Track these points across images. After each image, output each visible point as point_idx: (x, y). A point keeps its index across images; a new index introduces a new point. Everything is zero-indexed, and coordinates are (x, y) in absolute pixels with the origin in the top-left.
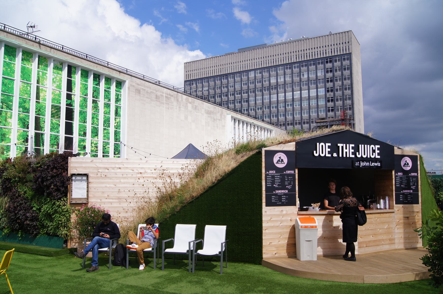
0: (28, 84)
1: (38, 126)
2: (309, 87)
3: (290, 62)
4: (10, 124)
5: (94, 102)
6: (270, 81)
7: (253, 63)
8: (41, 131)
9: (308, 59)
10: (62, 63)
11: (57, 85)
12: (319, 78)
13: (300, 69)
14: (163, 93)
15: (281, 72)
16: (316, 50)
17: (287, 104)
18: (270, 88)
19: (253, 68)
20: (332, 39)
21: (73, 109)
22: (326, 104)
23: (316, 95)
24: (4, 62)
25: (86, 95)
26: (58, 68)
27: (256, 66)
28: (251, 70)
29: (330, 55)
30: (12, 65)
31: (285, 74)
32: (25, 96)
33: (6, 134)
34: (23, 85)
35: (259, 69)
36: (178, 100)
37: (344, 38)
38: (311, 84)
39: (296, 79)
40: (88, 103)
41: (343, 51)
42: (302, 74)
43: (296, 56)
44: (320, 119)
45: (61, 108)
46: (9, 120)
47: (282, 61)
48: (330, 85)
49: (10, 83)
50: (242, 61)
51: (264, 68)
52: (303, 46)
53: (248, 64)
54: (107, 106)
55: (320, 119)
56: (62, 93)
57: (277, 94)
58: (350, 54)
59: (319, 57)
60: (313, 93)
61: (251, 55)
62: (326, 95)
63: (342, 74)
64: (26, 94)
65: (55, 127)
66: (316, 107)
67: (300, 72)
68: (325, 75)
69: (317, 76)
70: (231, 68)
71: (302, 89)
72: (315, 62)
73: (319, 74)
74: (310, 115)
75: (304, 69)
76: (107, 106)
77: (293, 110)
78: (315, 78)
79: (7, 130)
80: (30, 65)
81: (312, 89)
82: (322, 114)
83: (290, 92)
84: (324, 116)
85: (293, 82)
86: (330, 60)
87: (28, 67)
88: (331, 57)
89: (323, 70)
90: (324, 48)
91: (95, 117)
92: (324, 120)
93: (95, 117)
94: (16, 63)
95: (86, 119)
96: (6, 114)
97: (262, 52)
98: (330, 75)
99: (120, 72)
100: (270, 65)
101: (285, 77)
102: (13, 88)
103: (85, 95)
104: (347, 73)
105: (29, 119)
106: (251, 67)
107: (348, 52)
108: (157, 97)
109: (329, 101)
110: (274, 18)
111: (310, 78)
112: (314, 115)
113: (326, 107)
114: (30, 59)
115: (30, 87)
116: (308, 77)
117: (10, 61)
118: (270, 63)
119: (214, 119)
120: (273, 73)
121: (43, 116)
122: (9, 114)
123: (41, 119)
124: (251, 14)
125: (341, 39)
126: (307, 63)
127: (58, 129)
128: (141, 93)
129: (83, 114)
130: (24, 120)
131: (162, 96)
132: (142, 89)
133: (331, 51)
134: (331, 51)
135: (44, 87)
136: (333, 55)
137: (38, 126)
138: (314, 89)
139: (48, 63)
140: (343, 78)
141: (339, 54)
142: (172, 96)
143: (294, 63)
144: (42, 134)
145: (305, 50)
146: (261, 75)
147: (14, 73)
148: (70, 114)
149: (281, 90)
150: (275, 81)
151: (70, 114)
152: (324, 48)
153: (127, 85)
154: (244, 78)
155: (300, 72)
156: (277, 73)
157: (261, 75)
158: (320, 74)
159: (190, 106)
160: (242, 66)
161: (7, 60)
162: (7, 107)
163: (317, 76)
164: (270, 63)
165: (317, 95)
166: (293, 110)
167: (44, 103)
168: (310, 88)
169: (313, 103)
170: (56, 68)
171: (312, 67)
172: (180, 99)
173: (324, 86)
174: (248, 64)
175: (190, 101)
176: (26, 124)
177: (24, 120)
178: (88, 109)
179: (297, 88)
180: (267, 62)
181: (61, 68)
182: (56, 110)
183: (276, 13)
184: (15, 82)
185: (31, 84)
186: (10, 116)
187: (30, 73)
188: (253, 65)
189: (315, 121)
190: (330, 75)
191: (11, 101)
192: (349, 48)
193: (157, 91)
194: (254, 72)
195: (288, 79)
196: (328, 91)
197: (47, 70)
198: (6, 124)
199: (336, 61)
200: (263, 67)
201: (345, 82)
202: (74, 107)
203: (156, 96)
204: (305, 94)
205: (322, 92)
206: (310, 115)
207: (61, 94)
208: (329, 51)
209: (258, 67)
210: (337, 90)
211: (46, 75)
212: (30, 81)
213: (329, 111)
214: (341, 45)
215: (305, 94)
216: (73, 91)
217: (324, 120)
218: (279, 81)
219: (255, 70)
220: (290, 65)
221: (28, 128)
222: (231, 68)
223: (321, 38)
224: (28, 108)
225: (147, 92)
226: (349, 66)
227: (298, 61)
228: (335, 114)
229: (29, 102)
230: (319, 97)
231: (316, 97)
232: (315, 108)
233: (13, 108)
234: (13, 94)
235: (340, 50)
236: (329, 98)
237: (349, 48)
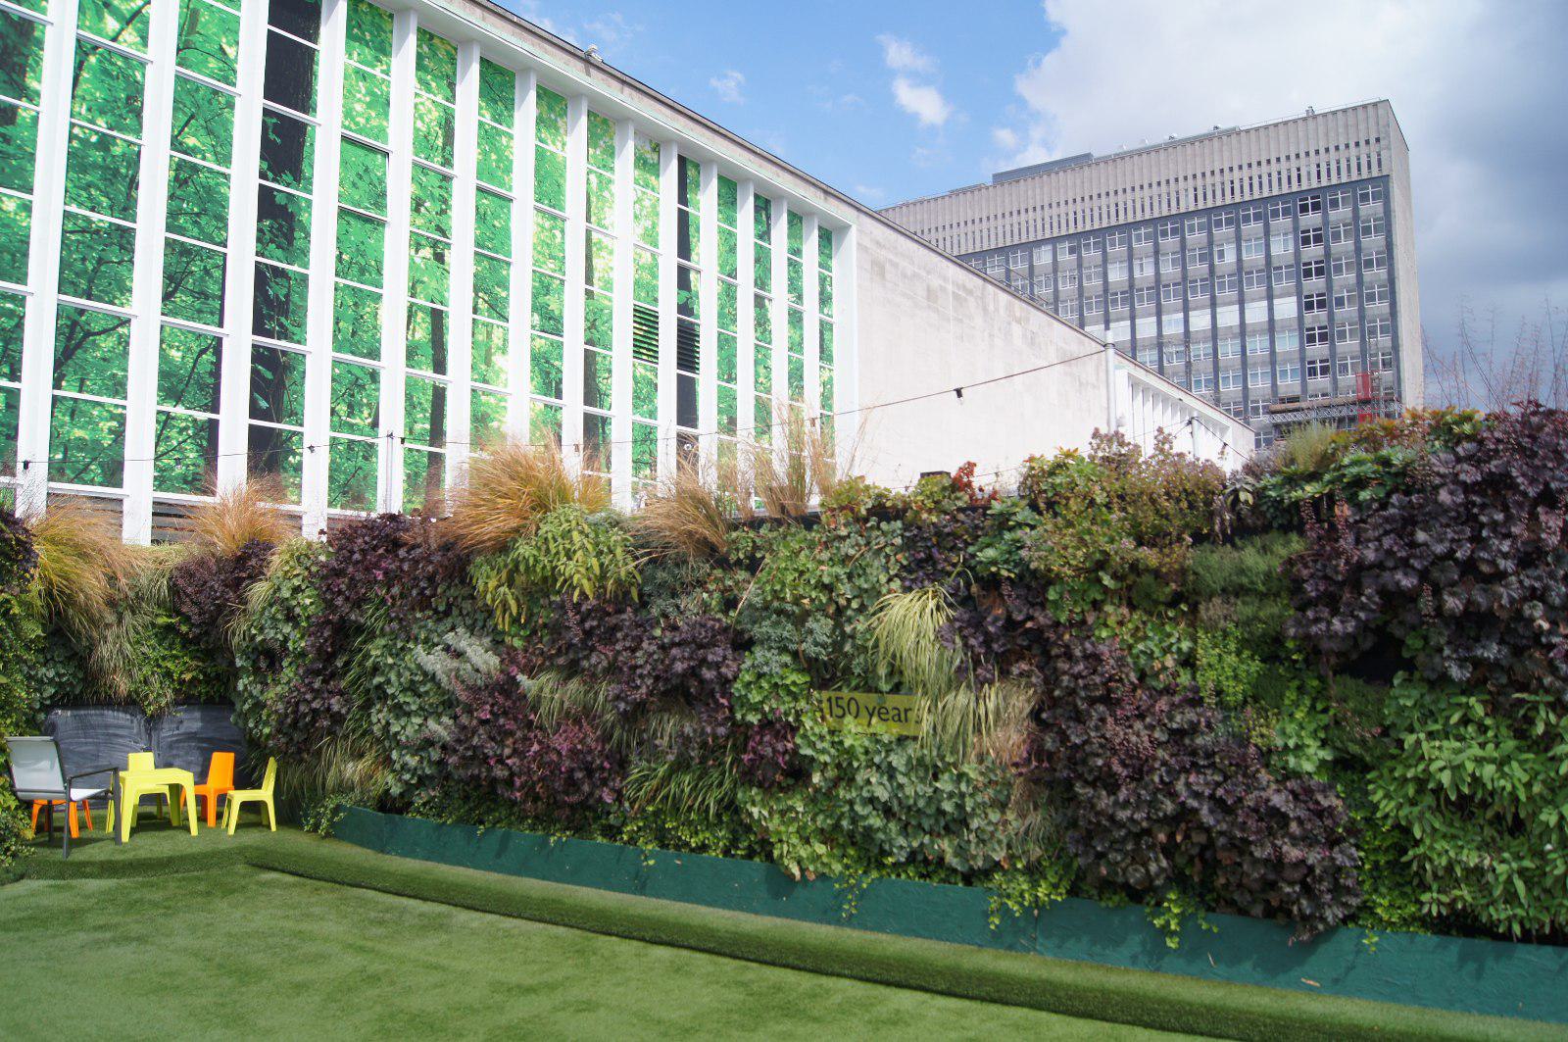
0: (554, 217)
1: (593, 393)
2: (1241, 293)
3: (1174, 212)
4: (503, 376)
5: (759, 302)
6: (1105, 275)
7: (1047, 219)
8: (601, 407)
9: (1238, 199)
10: (658, 145)
11: (646, 229)
12: (1275, 264)
13: (1210, 234)
14: (945, 279)
15: (1143, 246)
16: (1264, 168)
19: (1047, 236)
20: (1321, 130)
21: (692, 323)
22: (1302, 350)
23: (1265, 318)
24: (481, 124)
25: (733, 274)
26: (645, 162)
27: (1001, 239)
28: (1039, 243)
29: (1315, 184)
30: (504, 140)
31: (1157, 252)
32: (548, 268)
33: (488, 415)
34: (540, 221)
35: (1069, 237)
36: (985, 310)
37: (1362, 127)
40: (739, 304)
41: (1359, 169)
42: (1216, 249)
44: (1282, 401)
45: (660, 320)
46: (497, 359)
47: (1071, 223)
48: (1314, 284)
49: (498, 210)
50: (1007, 214)
51: (1086, 234)
52: (1216, 157)
53: (1031, 222)
54: (796, 318)
55: (1282, 401)
56: (660, 260)
57: (1133, 319)
58: (1385, 179)
59: (1275, 192)
60: (1256, 313)
61: (1038, 191)
62: (1300, 318)
63: (1358, 249)
64: (552, 257)
65: (644, 394)
66: (1268, 359)
67: (1211, 243)
68: (1297, 253)
69: (1268, 256)
70: (970, 235)
72: (1264, 209)
73: (1277, 249)
74: (1274, 385)
75: (1224, 232)
76: (796, 318)
79: (491, 399)
80: (559, 145)
81: (1253, 300)
82: (1289, 385)
83: (1177, 311)
84: (1297, 391)
85: (1184, 277)
86: (1315, 200)
87: (552, 153)
88: (1316, 193)
89: (1291, 236)
90: (1294, 163)
91: (762, 360)
92: (1296, 405)
93: (762, 360)
94: (515, 131)
95: (735, 366)
96: (489, 335)
97: (1078, 182)
98: (1313, 252)
99: (826, 192)
100: (1105, 225)
101: (1157, 264)
102: (506, 230)
103: (729, 275)
104: (1373, 243)
105: (560, 357)
106: (1016, 237)
107: (1375, 173)
108: (930, 294)
109: (1311, 339)
110: (1021, 102)
111: (1245, 265)
112: (1259, 385)
113: (1302, 359)
114: (560, 123)
115: (562, 231)
116: (1239, 260)
117: (496, 121)
118: (1105, 216)
119: (1081, 384)
120: (1117, 250)
121: (605, 347)
122: (497, 334)
123: (599, 359)
124: (948, 94)
125: (1352, 130)
126: (1235, 213)
127: (651, 401)
128: (888, 276)
129: (726, 344)
130: (547, 362)
131: (943, 289)
132: (891, 261)
133: (1319, 172)
134: (1319, 172)
135: (606, 235)
136: (1324, 183)
137: (593, 393)
138: (1261, 299)
139: (616, 143)
140: (1361, 263)
141: (1344, 180)
142: (970, 292)
143: (1189, 214)
144: (604, 421)
145: (1226, 171)
146: (1074, 257)
147: (508, 171)
148: (687, 339)
149: (1145, 306)
150: (1125, 277)
151: (687, 339)
152: (1294, 163)
153: (853, 236)
154: (1019, 266)
155: (1211, 243)
156: (1130, 249)
157: (1074, 257)
158: (1282, 248)
159: (1016, 329)
160: (1008, 228)
161: (487, 119)
162: (491, 306)
163: (1268, 256)
164: (1105, 216)
165: (1187, 331)
167: (606, 297)
168: (1138, 313)
169: (1258, 346)
170: (641, 163)
171: (1254, 228)
172: (991, 308)
173: (1293, 290)
174: (1031, 222)
175: (1018, 314)
176: (552, 376)
177: (547, 362)
178: (738, 329)
181: (653, 165)
182: (646, 321)
183: (1024, 87)
184: (514, 206)
185: (564, 220)
186: (500, 343)
187: (561, 176)
188: (1047, 226)
189: (1264, 407)
190: (1313, 252)
191: (504, 284)
192: (1379, 161)
193: (928, 273)
194: (1050, 247)
195: (1169, 271)
196: (1309, 306)
197: (612, 169)
198: (490, 375)
199: (1334, 204)
200: (1080, 230)
201: (1368, 275)
202: (698, 318)
203: (929, 290)
204: (1228, 317)
205: (1287, 308)
206: (1245, 388)
207: (657, 265)
209: (1063, 233)
210: (1340, 302)
211: (612, 187)
212: (562, 209)
213: (1312, 372)
214: (1353, 150)
215: (1228, 317)
216: (694, 256)
217: (1296, 405)
218: (1137, 274)
219: (1053, 241)
220: (1178, 221)
221: (559, 395)
222: (970, 235)
223: (1262, 132)
224: (557, 313)
225: (904, 276)
226: (1380, 219)
227: (1201, 206)
228: (1335, 381)
229: (561, 293)
230: (1278, 327)
231: (1266, 326)
232: (1263, 364)
233: (512, 311)
234: (508, 254)
235: (1349, 166)
237: (1379, 161)
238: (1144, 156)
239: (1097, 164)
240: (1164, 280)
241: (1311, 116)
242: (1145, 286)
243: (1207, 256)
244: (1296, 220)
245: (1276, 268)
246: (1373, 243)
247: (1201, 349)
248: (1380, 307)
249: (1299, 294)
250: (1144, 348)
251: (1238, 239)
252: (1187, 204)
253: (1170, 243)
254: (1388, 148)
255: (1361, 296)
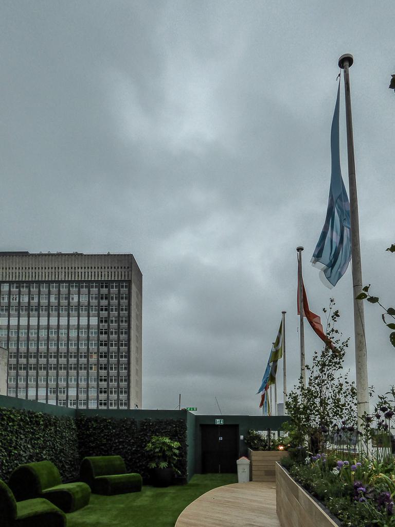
17: (91, 332)
18: (29, 308)
27: (120, 277)
38: (82, 311)
39: (64, 302)
43: (65, 273)
62: (98, 325)
71: (60, 315)
77: (58, 340)
78: (47, 304)
104: (124, 372)
113: (98, 340)
155: (69, 293)
165: (58, 325)
166: (58, 340)
179: (84, 313)
180: (27, 275)
196: (102, 321)
205: (94, 321)
208: (105, 275)
231: (86, 327)
236: (103, 330)
238: (44, 256)
239: (29, 256)
240: (41, 305)
241: (108, 255)
242: (44, 305)
243: (68, 298)
244: (99, 290)
245: (91, 306)
246: (123, 337)
247: (63, 332)
248: (124, 348)
249: (98, 316)
250: (42, 329)
251: (79, 294)
252: (62, 278)
253: (54, 290)
254: (131, 271)
255: (119, 320)
